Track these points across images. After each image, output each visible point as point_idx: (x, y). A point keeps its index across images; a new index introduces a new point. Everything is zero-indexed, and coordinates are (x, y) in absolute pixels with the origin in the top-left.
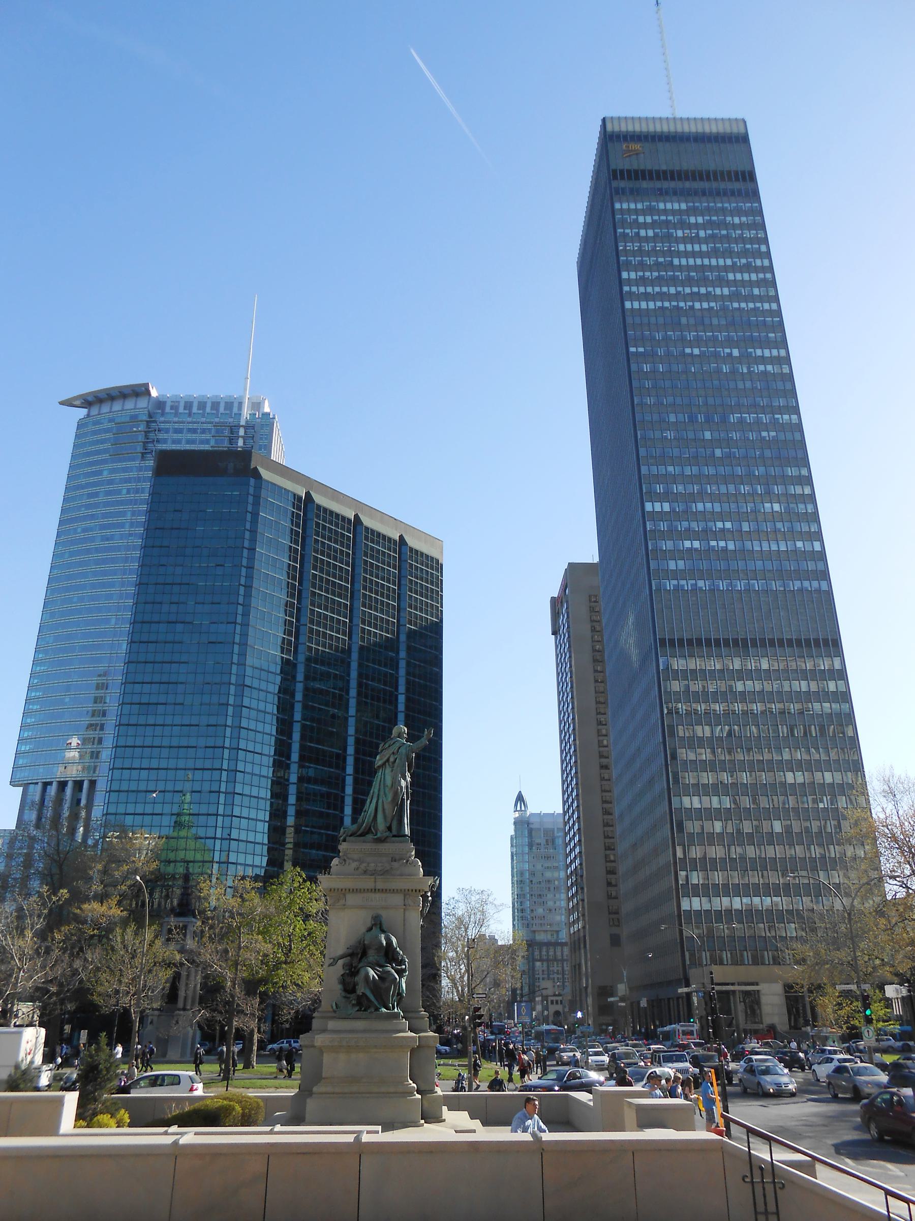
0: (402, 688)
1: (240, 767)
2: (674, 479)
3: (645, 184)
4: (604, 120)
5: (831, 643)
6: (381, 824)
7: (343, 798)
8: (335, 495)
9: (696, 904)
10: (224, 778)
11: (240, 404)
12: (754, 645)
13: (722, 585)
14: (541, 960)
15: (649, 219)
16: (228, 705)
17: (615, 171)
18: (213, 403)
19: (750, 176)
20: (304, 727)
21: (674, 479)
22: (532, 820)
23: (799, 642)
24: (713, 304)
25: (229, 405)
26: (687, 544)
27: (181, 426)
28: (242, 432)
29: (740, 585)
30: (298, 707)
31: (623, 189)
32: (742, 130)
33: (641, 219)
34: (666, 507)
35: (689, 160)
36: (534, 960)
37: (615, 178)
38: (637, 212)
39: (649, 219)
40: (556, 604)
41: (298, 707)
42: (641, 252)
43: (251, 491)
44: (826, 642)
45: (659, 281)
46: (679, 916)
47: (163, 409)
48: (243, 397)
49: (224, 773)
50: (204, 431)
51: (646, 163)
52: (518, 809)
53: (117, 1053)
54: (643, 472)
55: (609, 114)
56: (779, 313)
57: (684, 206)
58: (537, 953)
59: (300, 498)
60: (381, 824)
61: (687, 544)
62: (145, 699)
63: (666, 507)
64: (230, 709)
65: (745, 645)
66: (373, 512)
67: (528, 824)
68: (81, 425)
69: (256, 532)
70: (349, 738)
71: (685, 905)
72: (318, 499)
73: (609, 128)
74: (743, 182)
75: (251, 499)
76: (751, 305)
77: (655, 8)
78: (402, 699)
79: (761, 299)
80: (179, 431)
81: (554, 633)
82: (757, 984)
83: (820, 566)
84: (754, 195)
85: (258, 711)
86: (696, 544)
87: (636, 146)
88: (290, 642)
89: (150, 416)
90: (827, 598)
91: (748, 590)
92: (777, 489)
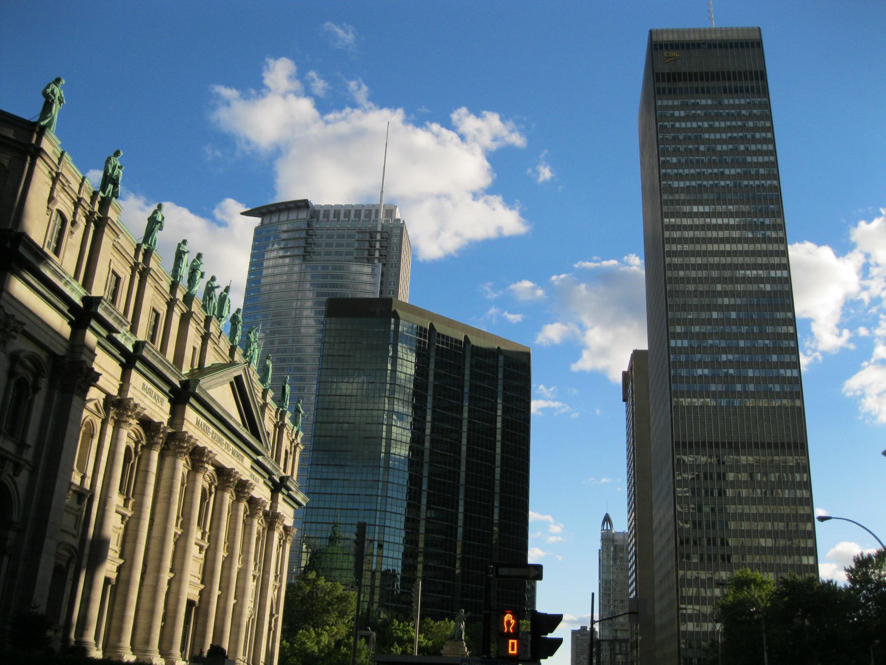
1: (387, 524)
2: (692, 322)
3: (681, 85)
4: (651, 31)
7: (456, 543)
8: (451, 323)
9: (690, 627)
10: (377, 531)
11: (377, 212)
13: (724, 402)
15: (682, 114)
16: (379, 481)
17: (658, 74)
18: (356, 211)
19: (762, 75)
20: (429, 495)
21: (692, 322)
22: (616, 538)
25: (369, 213)
26: (700, 372)
27: (337, 257)
28: (379, 237)
30: (425, 481)
31: (664, 89)
32: (758, 37)
33: (677, 114)
34: (686, 343)
37: (658, 80)
38: (674, 108)
39: (682, 114)
41: (425, 481)
42: (675, 140)
44: (796, 444)
45: (687, 164)
46: (679, 634)
47: (318, 218)
48: (380, 205)
49: (377, 528)
50: (350, 236)
54: (669, 316)
56: (778, 189)
58: (617, 647)
61: (700, 372)
62: (324, 476)
63: (686, 343)
64: (380, 484)
65: (737, 448)
66: (479, 333)
67: (613, 541)
68: (257, 231)
71: (683, 628)
73: (654, 39)
74: (755, 81)
76: (757, 182)
79: (763, 177)
80: (337, 253)
81: (624, 400)
83: (786, 288)
85: (399, 485)
86: (706, 371)
87: (674, 54)
89: (309, 225)
90: (799, 415)
91: (740, 407)
92: (769, 329)
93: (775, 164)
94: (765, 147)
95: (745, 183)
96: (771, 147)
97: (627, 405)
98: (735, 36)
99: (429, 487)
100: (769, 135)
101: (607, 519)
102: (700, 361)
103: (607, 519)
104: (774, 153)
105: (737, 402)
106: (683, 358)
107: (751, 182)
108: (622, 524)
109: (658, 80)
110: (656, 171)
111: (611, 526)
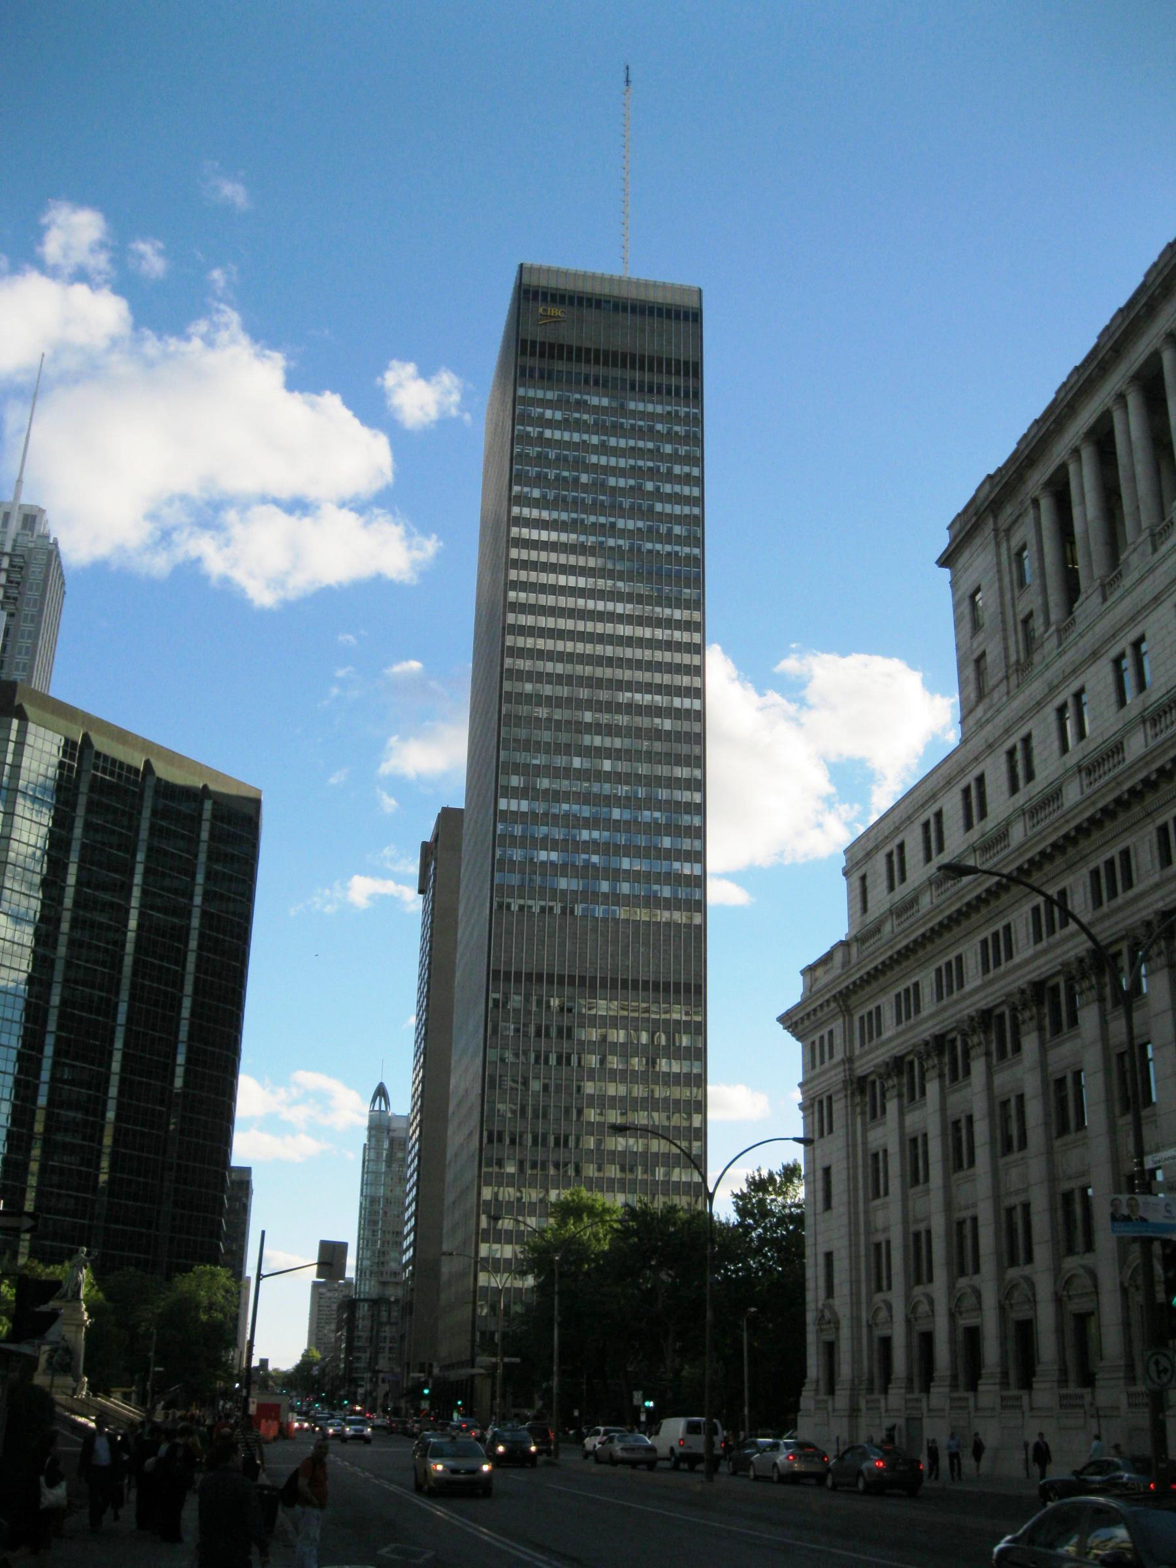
0: (188, 989)
2: (538, 771)
3: (561, 366)
5: (694, 991)
6: (70, 1294)
12: (604, 985)
14: (389, 1323)
19: (694, 369)
22: (394, 1125)
23: (656, 986)
24: (621, 542)
29: (599, 911)
34: (524, 806)
35: (624, 336)
36: (381, 1324)
40: (427, 851)
43: (13, 736)
51: (569, 336)
52: (377, 1108)
53: (1009, 1542)
55: (528, 261)
56: (699, 562)
57: (605, 402)
58: (384, 1314)
59: (74, 744)
60: (70, 1294)
67: (389, 1131)
69: (19, 767)
70: (115, 1052)
72: (100, 743)
73: (525, 280)
74: (683, 377)
75: (11, 746)
77: (623, 86)
78: (187, 1003)
79: (679, 540)
81: (421, 891)
82: (886, 1342)
84: (696, 396)
87: (556, 311)
88: (71, 767)
91: (605, 920)
93: (699, 521)
94: (686, 491)
95: (649, 546)
96: (696, 492)
97: (425, 900)
98: (658, 297)
99: (60, 1027)
100: (696, 472)
101: (381, 1092)
102: (546, 838)
103: (381, 1092)
104: (699, 501)
105: (599, 911)
106: (518, 830)
107: (658, 547)
108: (402, 1104)
109: (524, 353)
110: (504, 527)
111: (387, 1103)
